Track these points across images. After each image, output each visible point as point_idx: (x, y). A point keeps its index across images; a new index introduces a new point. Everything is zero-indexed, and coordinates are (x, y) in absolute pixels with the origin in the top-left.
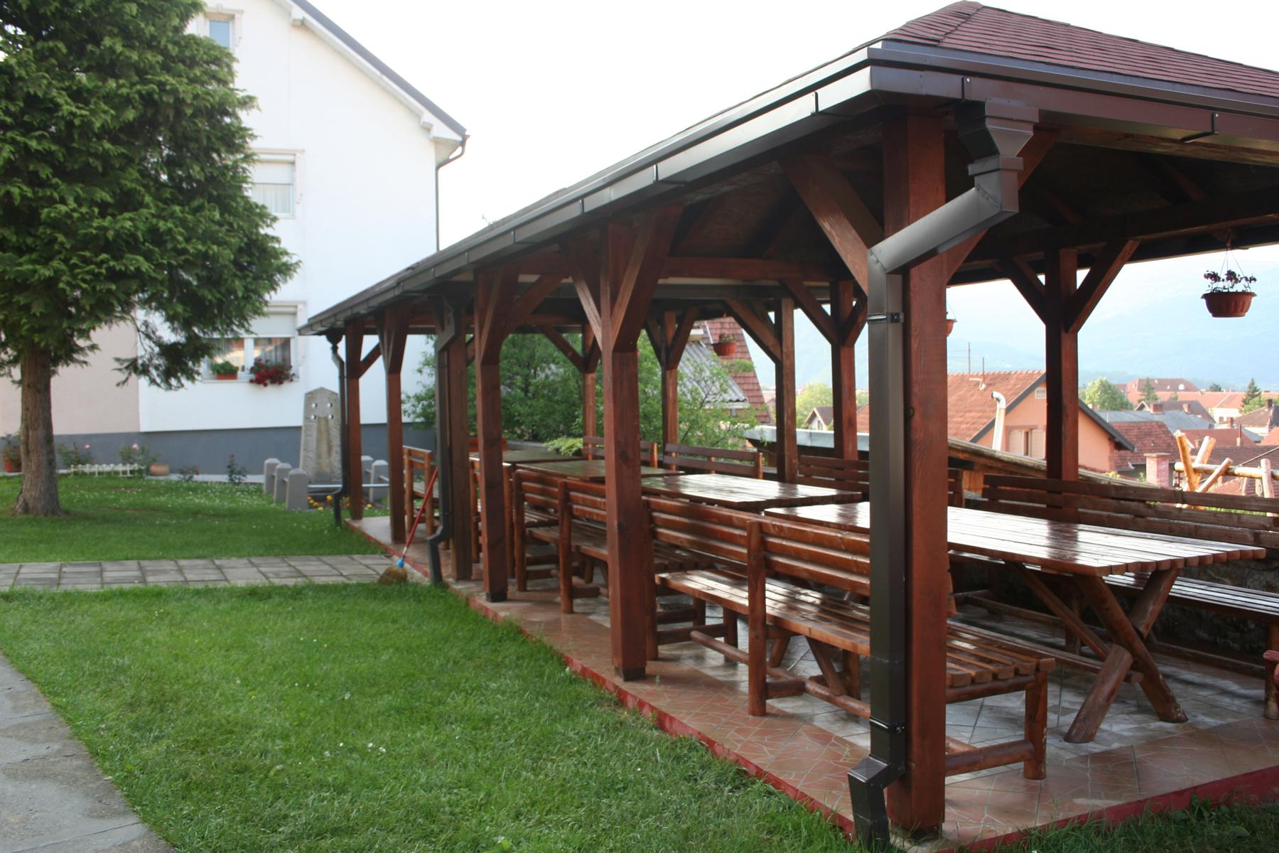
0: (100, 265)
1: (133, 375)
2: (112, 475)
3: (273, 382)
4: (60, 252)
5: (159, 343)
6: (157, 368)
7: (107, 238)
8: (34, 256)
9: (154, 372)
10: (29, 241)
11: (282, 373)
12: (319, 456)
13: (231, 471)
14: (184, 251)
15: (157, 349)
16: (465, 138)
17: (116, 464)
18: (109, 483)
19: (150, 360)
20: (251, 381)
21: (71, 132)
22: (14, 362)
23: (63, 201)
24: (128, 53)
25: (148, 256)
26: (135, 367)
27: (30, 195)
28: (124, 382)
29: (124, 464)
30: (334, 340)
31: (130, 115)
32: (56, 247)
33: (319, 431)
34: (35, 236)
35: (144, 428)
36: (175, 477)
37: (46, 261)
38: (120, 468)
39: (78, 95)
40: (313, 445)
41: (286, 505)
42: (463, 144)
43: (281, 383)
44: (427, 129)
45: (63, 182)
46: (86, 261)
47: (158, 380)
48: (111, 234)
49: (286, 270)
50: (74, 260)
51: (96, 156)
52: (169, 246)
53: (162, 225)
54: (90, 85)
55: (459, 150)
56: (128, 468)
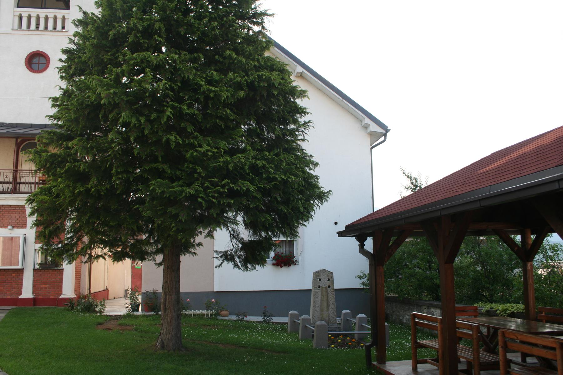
0: (223, 186)
1: (225, 261)
2: (201, 316)
3: (285, 265)
4: (197, 179)
5: (241, 241)
6: (239, 257)
7: (228, 169)
8: (181, 182)
9: (237, 260)
10: (178, 173)
11: (290, 260)
12: (322, 310)
13: (264, 314)
14: (274, 179)
15: (240, 246)
16: (387, 131)
17: (203, 310)
18: (202, 322)
19: (236, 252)
20: (273, 264)
21: (207, 100)
22: (158, 252)
23: (201, 146)
24: (240, 58)
25: (252, 182)
26: (227, 257)
27: (181, 142)
28: (220, 265)
29: (207, 310)
30: (361, 240)
31: (242, 94)
32: (196, 176)
33: (322, 295)
34: (181, 170)
35: (215, 290)
36: (234, 317)
37: (189, 185)
38: (205, 312)
39: (210, 82)
40: (319, 304)
41: (314, 343)
42: (385, 135)
43: (290, 266)
44: (366, 127)
45: (201, 135)
46: (214, 185)
47: (240, 265)
48: (231, 166)
49: (322, 196)
50: (207, 184)
51: (221, 118)
52: (264, 176)
54: (217, 78)
55: (382, 139)
56: (209, 312)
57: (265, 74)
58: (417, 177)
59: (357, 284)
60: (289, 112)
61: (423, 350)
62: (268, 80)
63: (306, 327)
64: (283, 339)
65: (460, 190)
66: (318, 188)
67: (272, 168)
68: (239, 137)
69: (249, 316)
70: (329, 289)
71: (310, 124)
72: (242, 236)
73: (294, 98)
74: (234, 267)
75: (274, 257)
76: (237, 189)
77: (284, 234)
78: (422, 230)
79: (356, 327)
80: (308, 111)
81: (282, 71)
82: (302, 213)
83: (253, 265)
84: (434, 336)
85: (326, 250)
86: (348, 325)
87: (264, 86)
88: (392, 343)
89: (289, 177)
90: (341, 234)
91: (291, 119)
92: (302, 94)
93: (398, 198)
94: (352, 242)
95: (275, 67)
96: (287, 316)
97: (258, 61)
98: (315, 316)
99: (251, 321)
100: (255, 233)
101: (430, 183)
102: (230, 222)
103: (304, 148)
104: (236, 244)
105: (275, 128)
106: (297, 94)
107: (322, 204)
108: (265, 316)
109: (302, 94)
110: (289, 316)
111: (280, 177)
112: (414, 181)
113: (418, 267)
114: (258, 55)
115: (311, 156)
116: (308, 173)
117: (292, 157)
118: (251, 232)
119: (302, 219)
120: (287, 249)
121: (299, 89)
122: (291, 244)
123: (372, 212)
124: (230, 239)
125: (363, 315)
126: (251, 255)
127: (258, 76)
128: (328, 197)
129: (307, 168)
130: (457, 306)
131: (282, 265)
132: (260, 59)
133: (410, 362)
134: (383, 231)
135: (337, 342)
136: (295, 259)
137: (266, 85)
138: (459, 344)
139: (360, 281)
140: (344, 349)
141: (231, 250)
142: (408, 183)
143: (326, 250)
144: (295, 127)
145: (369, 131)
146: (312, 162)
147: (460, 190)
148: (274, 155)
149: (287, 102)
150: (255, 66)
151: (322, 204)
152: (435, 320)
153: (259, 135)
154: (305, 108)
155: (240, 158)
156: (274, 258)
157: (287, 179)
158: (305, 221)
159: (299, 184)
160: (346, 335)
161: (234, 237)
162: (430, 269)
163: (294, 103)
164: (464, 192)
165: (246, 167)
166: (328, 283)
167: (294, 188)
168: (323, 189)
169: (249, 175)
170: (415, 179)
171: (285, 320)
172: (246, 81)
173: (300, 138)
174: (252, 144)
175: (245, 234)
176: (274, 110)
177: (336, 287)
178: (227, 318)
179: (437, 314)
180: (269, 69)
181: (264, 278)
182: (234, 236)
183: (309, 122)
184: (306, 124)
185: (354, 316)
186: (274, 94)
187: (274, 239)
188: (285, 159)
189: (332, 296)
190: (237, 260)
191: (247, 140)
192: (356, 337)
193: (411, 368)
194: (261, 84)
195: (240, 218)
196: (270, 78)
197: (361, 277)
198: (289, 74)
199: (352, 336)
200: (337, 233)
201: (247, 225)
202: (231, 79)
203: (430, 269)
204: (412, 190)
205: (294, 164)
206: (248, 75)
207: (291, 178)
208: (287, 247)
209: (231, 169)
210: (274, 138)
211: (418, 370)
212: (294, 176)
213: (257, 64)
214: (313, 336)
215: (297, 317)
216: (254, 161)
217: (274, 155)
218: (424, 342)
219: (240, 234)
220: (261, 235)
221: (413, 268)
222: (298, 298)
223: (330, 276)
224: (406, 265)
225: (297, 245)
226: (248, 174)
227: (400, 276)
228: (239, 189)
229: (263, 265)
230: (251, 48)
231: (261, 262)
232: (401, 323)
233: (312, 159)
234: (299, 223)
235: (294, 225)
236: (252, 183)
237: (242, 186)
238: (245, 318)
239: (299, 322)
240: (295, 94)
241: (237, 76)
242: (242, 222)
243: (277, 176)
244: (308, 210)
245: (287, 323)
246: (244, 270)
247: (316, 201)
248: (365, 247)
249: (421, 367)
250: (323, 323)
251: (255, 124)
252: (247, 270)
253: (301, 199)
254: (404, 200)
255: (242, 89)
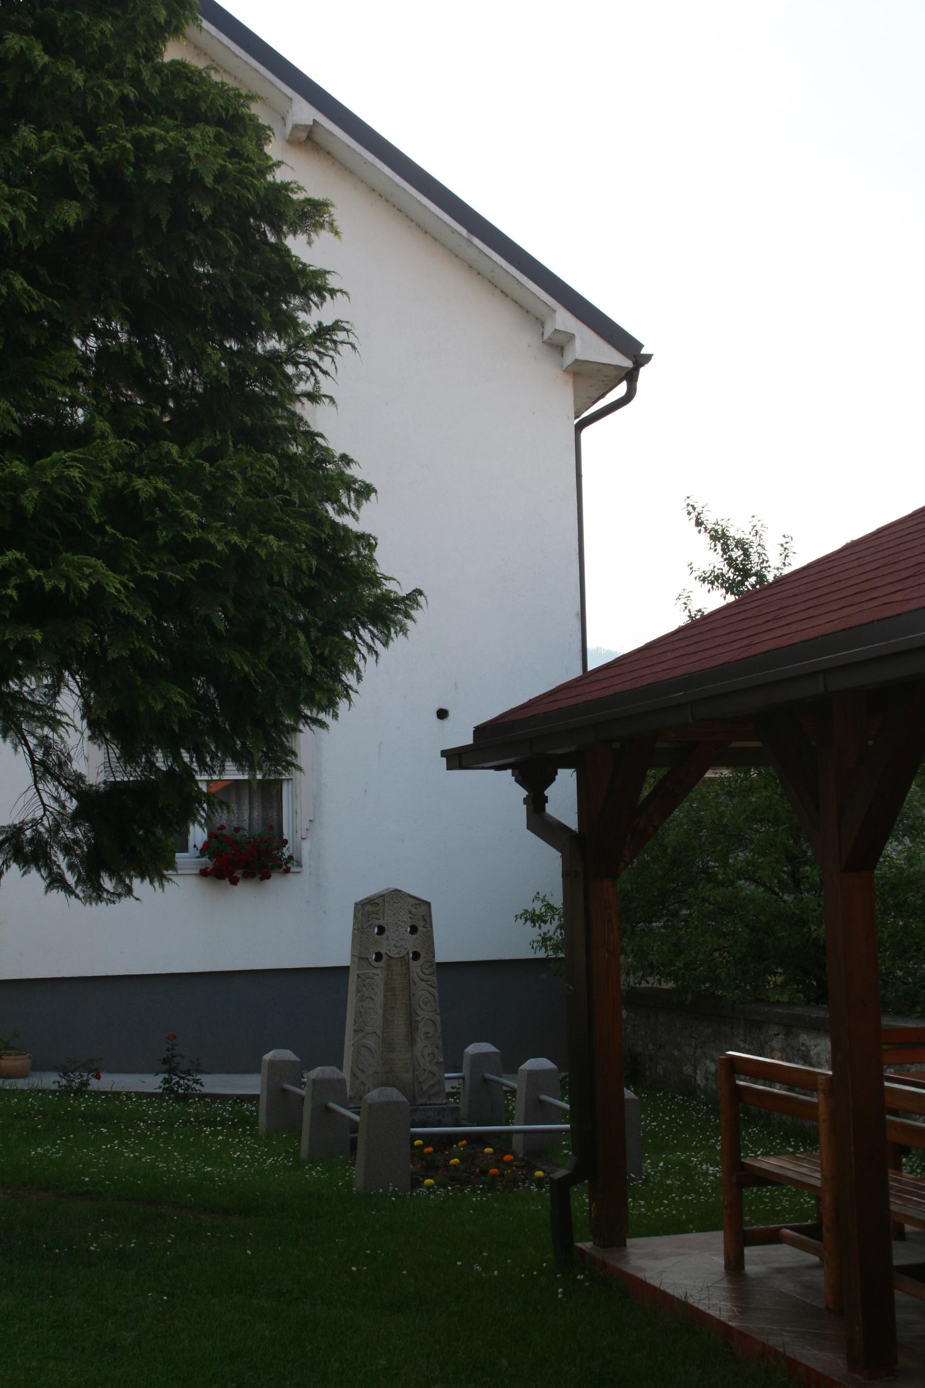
1: (14, 867)
3: (249, 875)
5: (76, 786)
6: (67, 849)
9: (61, 860)
13: (169, 1066)
15: (72, 805)
16: (640, 360)
19: (55, 829)
20: (204, 873)
30: (535, 782)
31: (71, 213)
33: (389, 988)
36: (50, 1080)
41: (357, 1174)
42: (631, 377)
43: (266, 876)
48: (30, 498)
49: (390, 614)
52: (163, 536)
53: (144, 487)
55: (621, 390)
57: (164, 133)
58: (747, 536)
59: (519, 943)
60: (258, 289)
61: (766, 1191)
62: (175, 158)
63: (329, 1110)
64: (239, 1161)
65: (899, 597)
66: (374, 580)
67: (191, 505)
68: (63, 382)
69: (110, 1071)
70: (415, 966)
71: (341, 336)
72: (78, 766)
73: (278, 232)
74: (49, 887)
75: (206, 846)
76: (56, 588)
77: (242, 759)
78: (758, 744)
79: (519, 1105)
80: (332, 282)
81: (233, 123)
82: (310, 680)
83: (121, 881)
84: (808, 1139)
85: (399, 814)
86: (488, 1101)
87: (161, 183)
88: (654, 1165)
89: (258, 541)
90: (457, 759)
91: (267, 316)
92: (312, 215)
93: (677, 620)
94: (500, 789)
95: (203, 106)
96: (259, 1072)
97: (136, 79)
98: (356, 1070)
99: (117, 1095)
100: (128, 757)
101: (798, 562)
102: (31, 718)
103: (315, 428)
104: (56, 799)
105: (204, 352)
106: (291, 214)
107: (386, 644)
108: (170, 1071)
109: (312, 215)
110: (265, 1069)
111: (223, 539)
112: (737, 553)
113: (750, 879)
114: (136, 54)
115: (346, 459)
116: (334, 525)
117: (269, 462)
118: (115, 751)
119: (311, 701)
120: (256, 814)
121: (298, 196)
122: (270, 793)
123: (578, 673)
124: (30, 780)
125: (542, 1063)
126: (114, 840)
127: (137, 141)
128: (408, 616)
129: (329, 507)
130: (887, 1022)
131: (238, 873)
132: (146, 75)
133: (717, 1238)
134: (616, 745)
135: (446, 1166)
136: (287, 852)
137: (168, 179)
138: (898, 1167)
139: (533, 932)
140: (473, 1192)
141: (35, 822)
142: (712, 560)
143: (399, 814)
144: (282, 347)
145: (569, 359)
146: (349, 484)
147: (899, 597)
148: (198, 456)
149: (253, 246)
150: (124, 99)
151: (386, 644)
152: (807, 1082)
153: (146, 380)
154: (323, 273)
155: (63, 464)
156: (206, 849)
157: (251, 548)
158: (322, 708)
159: (297, 568)
160: (481, 1140)
161: (47, 770)
162: (797, 883)
163: (282, 251)
164: (911, 606)
165: (92, 502)
166: (411, 943)
167: (281, 583)
168: (389, 585)
169: (104, 533)
170: (740, 544)
171: (249, 1084)
172: (88, 159)
173: (303, 387)
174: (117, 413)
175: (92, 761)
176: (199, 277)
177: (441, 956)
178: (21, 1084)
179: (819, 1057)
180: (180, 115)
181: (168, 926)
182: (49, 767)
183: (337, 326)
184: (324, 334)
185: (511, 1068)
186: (198, 216)
187: (201, 777)
188: (243, 471)
189: (426, 993)
190: (61, 860)
191: (96, 395)
192: (518, 1144)
193: (721, 1260)
194: (149, 175)
195: (69, 702)
196: (182, 150)
197: (534, 918)
198: (261, 134)
199: (502, 1141)
200: (444, 753)
201: (98, 728)
202: (26, 150)
203: (797, 883)
204: (731, 587)
205: (278, 491)
206: (94, 138)
207: (266, 544)
208: (257, 804)
209: (30, 507)
210: (200, 389)
211: (749, 1268)
212: (279, 537)
213: (131, 92)
214: (354, 1144)
215: (295, 1072)
216: (121, 479)
217: (198, 456)
218: (771, 1163)
219: (70, 758)
220: (151, 764)
221: (732, 884)
222: (294, 999)
223: (419, 915)
224: (705, 870)
225: (294, 796)
226: (99, 529)
227: (685, 912)
228: (63, 586)
229: (162, 878)
230: (108, 26)
231: (156, 866)
232: (690, 1090)
233: (348, 472)
234: (299, 716)
235: (278, 724)
236: (113, 566)
237: (73, 574)
238: (93, 1081)
239: (303, 1092)
240: (281, 216)
241: (52, 141)
242: (78, 714)
243: (212, 538)
244: (335, 664)
245: (256, 1097)
246: (88, 899)
247: (364, 633)
248: (550, 809)
249: (757, 1259)
250: (394, 1094)
251: (130, 333)
252: (99, 898)
253: (305, 627)
254: (700, 628)
255: (74, 195)
